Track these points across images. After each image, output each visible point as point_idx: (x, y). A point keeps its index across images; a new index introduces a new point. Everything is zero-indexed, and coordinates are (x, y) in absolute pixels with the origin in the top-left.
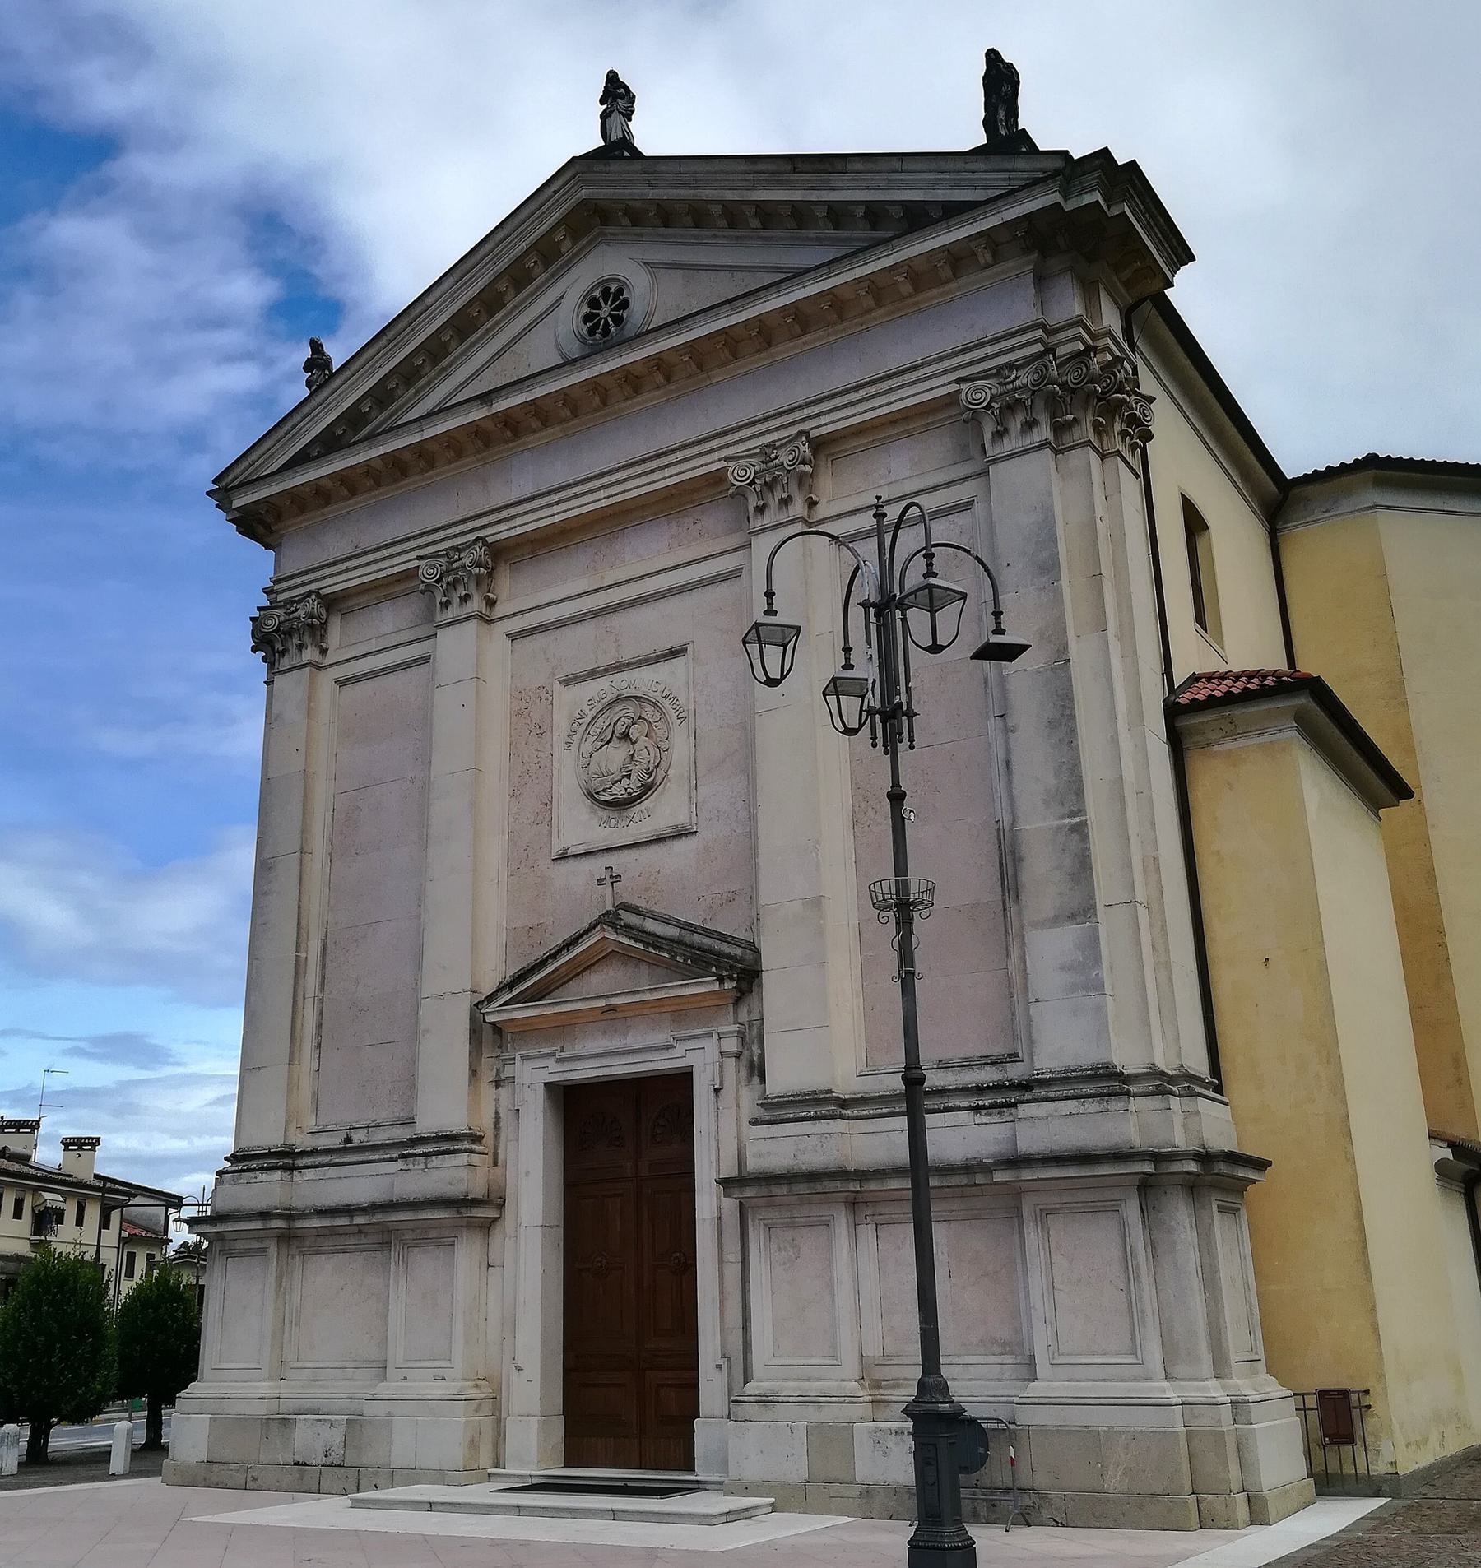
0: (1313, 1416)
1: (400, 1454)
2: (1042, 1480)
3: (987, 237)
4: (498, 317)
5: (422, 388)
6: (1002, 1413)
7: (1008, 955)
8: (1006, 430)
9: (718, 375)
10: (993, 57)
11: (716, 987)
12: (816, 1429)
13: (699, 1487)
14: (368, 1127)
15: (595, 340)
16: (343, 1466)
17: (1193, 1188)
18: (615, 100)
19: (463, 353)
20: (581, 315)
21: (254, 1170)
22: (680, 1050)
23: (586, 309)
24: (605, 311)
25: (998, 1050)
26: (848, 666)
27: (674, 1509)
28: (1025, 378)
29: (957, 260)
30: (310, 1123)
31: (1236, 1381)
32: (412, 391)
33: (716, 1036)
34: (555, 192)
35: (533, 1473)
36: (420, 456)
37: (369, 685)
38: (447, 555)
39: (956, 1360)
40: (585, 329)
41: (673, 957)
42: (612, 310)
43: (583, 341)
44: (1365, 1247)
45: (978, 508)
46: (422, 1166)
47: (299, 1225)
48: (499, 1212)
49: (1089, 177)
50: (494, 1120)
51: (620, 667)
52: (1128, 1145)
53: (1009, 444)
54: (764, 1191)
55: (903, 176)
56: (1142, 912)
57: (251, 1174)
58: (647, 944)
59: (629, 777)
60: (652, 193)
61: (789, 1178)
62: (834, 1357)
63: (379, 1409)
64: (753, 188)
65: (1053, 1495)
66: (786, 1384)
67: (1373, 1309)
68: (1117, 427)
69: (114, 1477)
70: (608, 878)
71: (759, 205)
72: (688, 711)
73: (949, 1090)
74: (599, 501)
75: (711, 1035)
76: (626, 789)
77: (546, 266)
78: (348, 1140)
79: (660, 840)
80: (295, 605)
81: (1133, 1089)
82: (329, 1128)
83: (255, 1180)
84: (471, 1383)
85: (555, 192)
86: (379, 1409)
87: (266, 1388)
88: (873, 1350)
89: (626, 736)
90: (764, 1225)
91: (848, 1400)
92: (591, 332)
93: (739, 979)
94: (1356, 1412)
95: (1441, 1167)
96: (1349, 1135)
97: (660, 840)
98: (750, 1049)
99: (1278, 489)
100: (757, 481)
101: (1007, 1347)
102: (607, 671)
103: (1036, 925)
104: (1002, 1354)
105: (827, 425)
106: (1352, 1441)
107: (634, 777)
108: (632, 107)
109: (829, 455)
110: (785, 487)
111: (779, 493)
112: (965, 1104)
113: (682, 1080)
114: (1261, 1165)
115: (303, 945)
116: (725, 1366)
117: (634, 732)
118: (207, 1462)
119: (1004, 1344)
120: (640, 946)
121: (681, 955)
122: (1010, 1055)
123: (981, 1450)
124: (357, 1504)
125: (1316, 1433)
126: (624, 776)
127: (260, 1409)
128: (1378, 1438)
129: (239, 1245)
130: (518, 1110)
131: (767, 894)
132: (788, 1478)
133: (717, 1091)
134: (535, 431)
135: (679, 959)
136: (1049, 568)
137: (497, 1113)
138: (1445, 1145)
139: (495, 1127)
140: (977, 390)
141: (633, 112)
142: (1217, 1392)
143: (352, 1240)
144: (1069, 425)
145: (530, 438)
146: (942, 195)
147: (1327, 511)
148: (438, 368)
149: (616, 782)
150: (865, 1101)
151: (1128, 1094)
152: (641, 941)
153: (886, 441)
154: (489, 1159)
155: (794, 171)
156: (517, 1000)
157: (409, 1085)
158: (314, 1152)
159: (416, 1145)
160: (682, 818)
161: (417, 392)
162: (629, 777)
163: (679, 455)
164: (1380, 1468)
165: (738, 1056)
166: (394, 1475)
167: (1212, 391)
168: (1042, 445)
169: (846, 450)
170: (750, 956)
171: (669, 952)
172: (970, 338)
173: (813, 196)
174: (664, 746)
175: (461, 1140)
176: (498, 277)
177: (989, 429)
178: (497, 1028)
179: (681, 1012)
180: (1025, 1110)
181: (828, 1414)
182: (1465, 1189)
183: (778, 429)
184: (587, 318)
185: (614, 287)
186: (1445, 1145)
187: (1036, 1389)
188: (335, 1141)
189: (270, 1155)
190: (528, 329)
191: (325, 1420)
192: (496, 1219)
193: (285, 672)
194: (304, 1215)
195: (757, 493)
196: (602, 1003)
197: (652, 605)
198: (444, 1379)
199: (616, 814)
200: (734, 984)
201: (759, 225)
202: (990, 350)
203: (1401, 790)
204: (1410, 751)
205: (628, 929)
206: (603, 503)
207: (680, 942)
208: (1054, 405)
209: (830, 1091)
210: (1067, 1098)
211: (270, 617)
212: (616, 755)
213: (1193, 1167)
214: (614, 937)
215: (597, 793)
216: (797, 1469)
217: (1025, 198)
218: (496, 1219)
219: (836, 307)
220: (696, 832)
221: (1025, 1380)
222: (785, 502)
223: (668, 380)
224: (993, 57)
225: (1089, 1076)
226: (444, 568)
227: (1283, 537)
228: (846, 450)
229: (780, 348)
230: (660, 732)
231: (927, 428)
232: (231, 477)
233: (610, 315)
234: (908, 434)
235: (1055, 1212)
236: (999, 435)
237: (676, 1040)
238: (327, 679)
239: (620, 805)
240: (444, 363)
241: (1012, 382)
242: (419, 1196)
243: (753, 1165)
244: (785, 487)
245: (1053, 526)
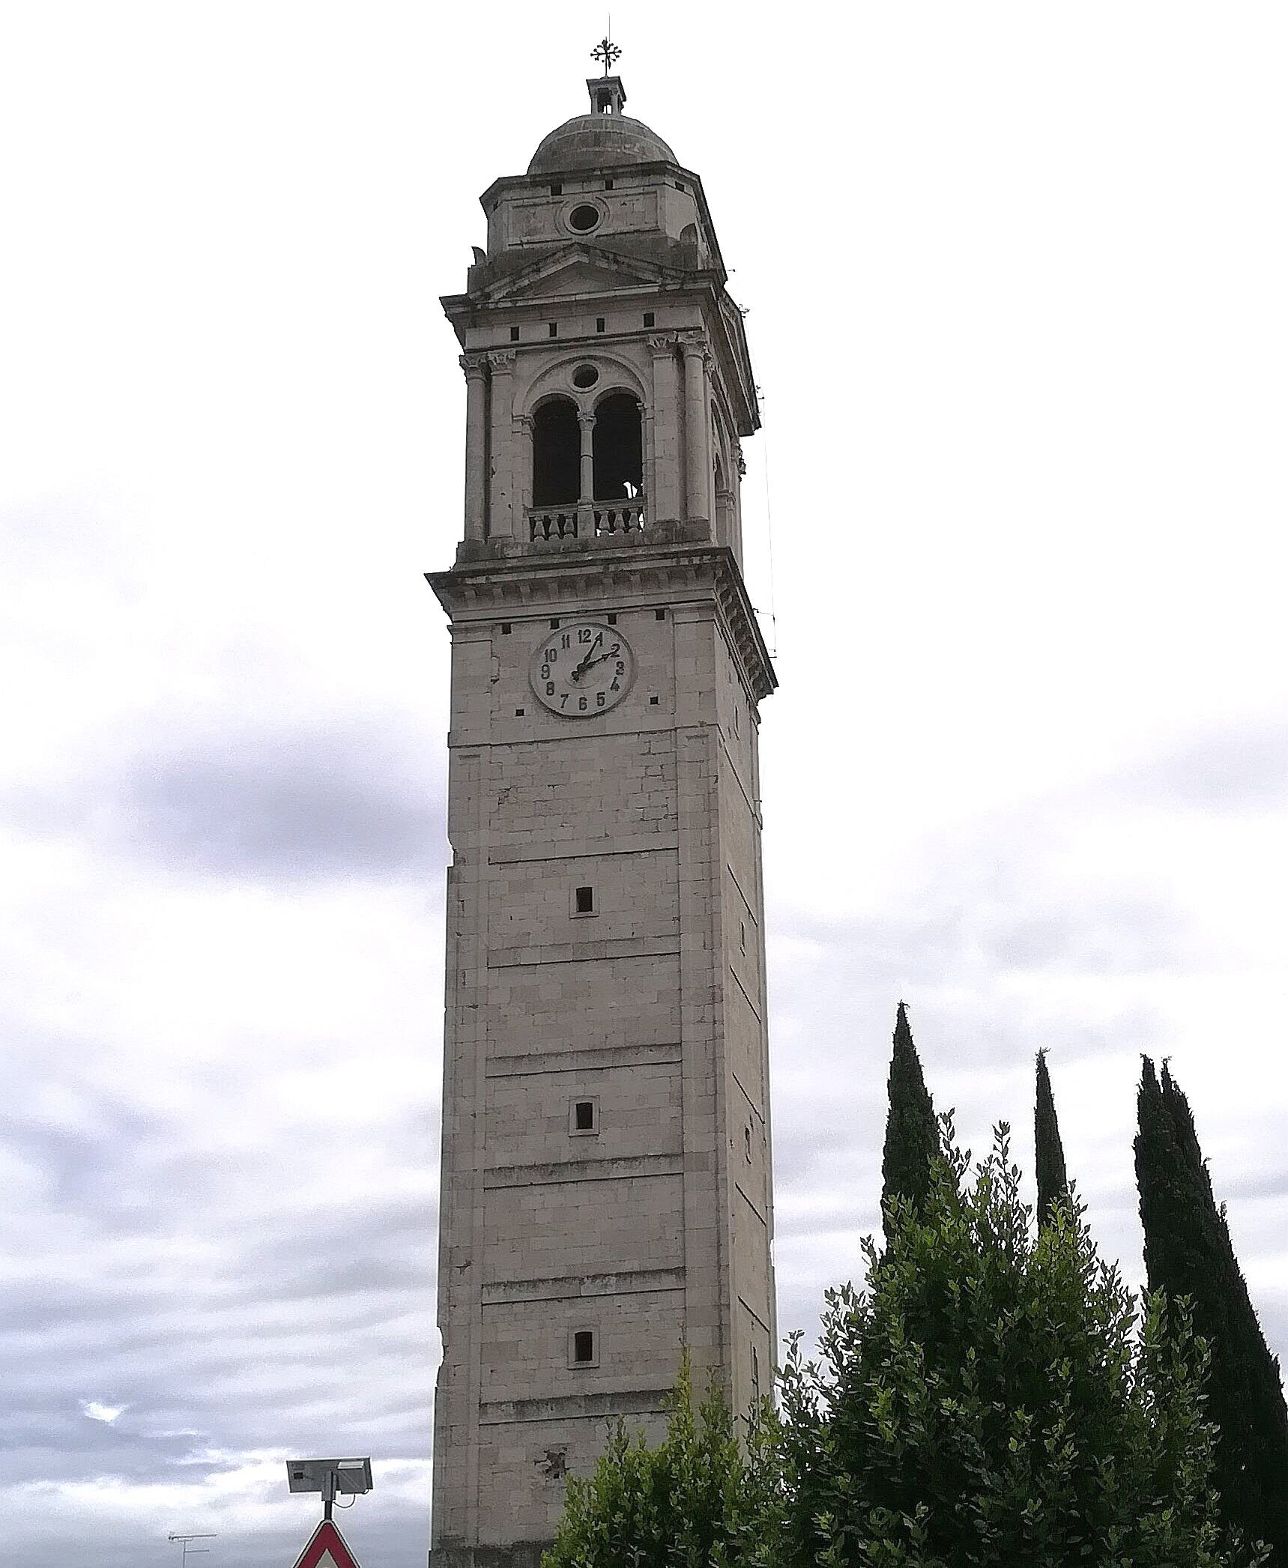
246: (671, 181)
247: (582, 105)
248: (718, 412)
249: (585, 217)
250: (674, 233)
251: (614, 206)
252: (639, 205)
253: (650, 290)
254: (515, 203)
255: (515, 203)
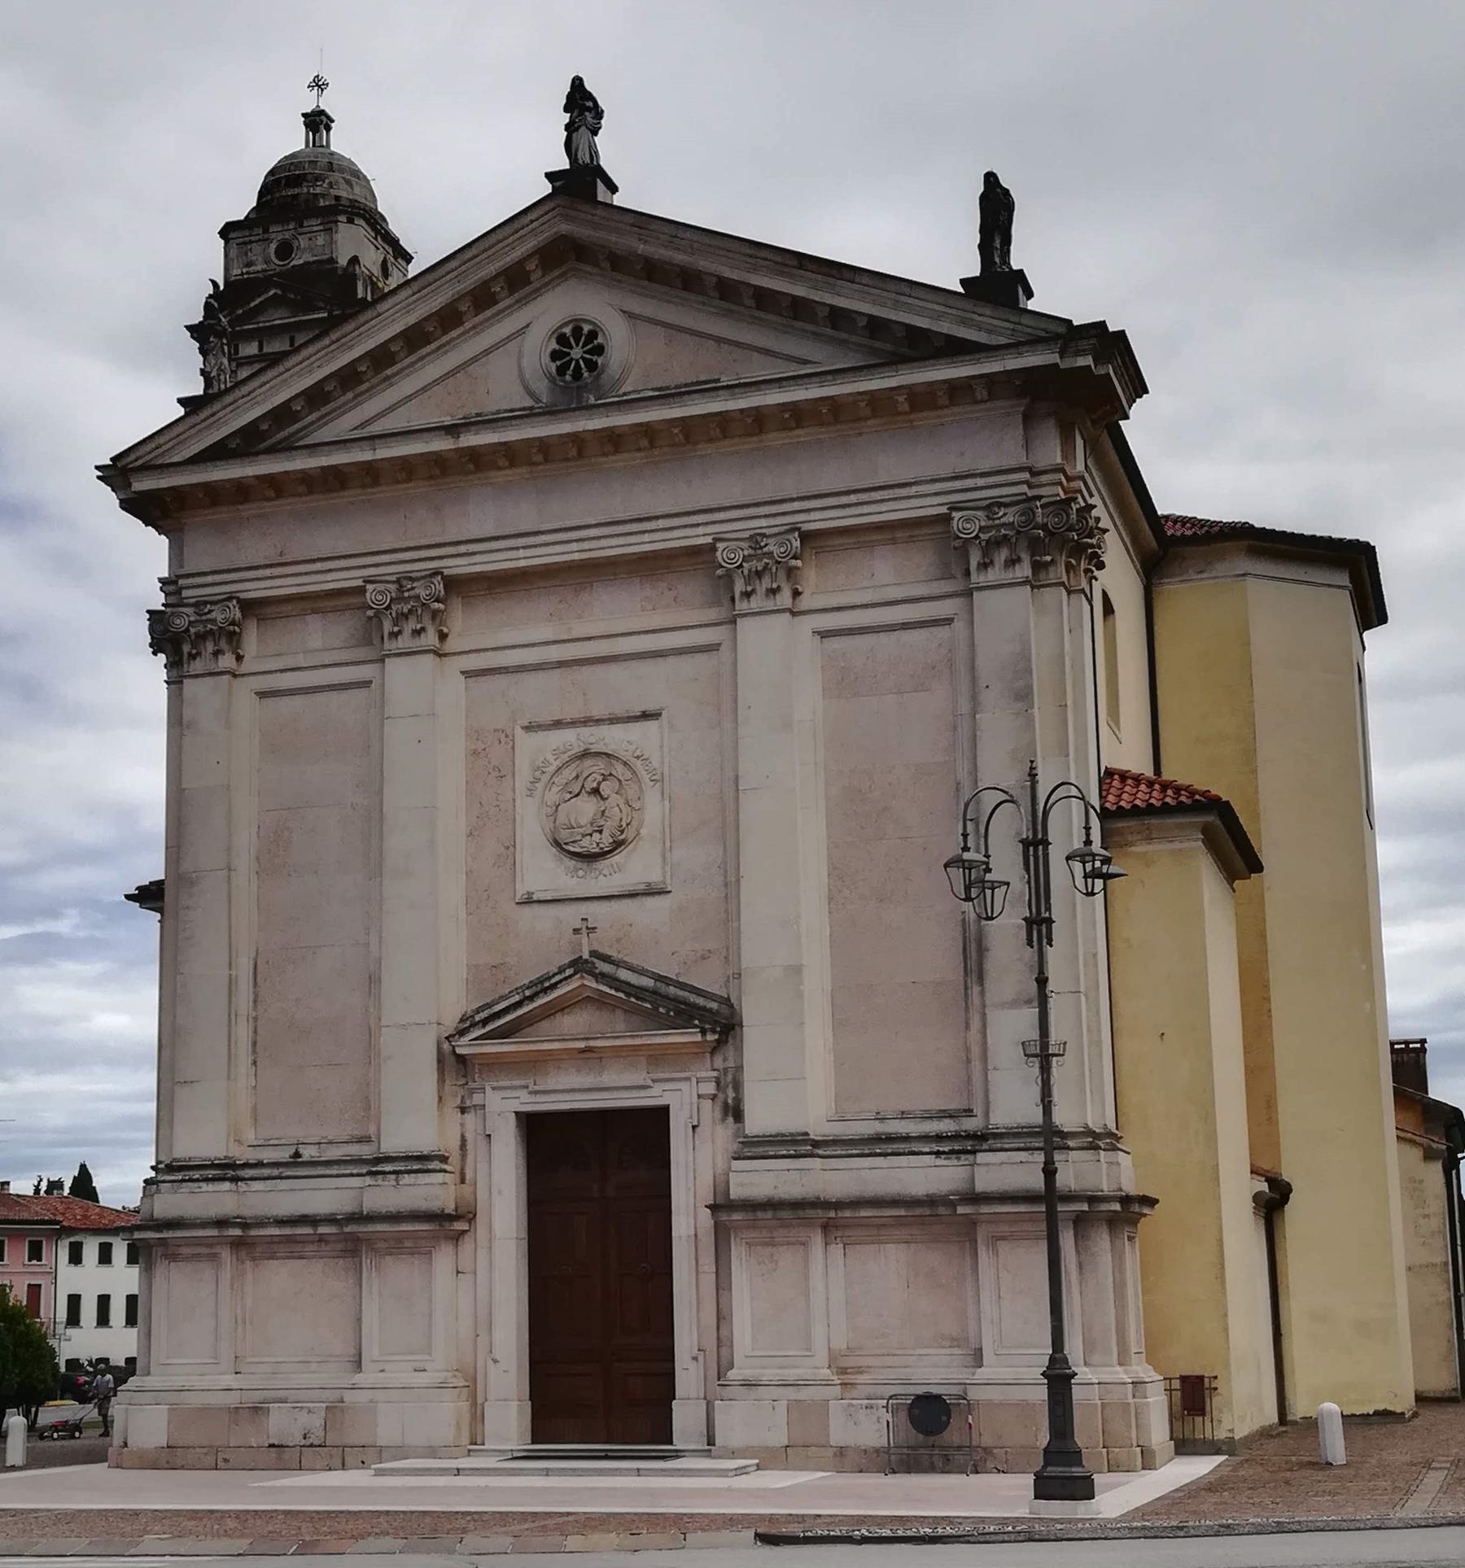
0: (1177, 1395)
1: (386, 1434)
2: (987, 1440)
3: (990, 381)
4: (454, 334)
5: (362, 393)
6: (955, 1390)
7: (967, 1026)
8: (992, 562)
9: (704, 449)
10: (991, 179)
11: (699, 1038)
12: (793, 1406)
13: (677, 1454)
14: (320, 1143)
15: (564, 381)
16: (325, 1446)
17: (1114, 1222)
18: (581, 114)
19: (412, 364)
20: (549, 350)
21: (197, 1180)
22: (657, 1089)
23: (554, 345)
24: (577, 353)
25: (952, 1106)
26: (966, 849)
27: (679, 1466)
28: (1010, 516)
29: (957, 391)
30: (250, 1136)
31: (1135, 1367)
32: (350, 395)
33: (694, 1080)
34: (532, 221)
35: (514, 1448)
36: (368, 473)
37: (297, 701)
38: (398, 581)
39: (911, 1352)
40: (553, 367)
41: (656, 1009)
42: (584, 352)
43: (552, 380)
44: (1223, 1267)
45: (959, 625)
46: (394, 1183)
47: (253, 1232)
48: (467, 1224)
49: (1085, 342)
50: (459, 1143)
51: (587, 721)
52: (1067, 1189)
53: (993, 575)
54: (750, 1216)
55: (910, 300)
56: (1083, 998)
57: (196, 1185)
58: (628, 994)
59: (601, 832)
60: (641, 248)
61: (772, 1205)
62: (809, 1349)
63: (362, 1397)
64: (754, 269)
65: (995, 1451)
66: (764, 1371)
67: (1226, 1315)
68: (1083, 566)
69: (13, 1468)
70: (584, 929)
71: (758, 289)
72: (662, 774)
73: (912, 1137)
74: (573, 553)
75: (688, 1079)
76: (598, 844)
77: (511, 293)
78: (297, 1155)
79: (632, 895)
80: (209, 606)
81: (1071, 1143)
82: (271, 1142)
83: (199, 1190)
84: (451, 1374)
85: (532, 221)
86: (362, 1397)
87: (229, 1380)
88: (840, 1344)
89: (596, 791)
90: (747, 1243)
91: (824, 1383)
92: (561, 371)
93: (720, 1033)
94: (1207, 1392)
95: (1257, 1197)
96: (1217, 1179)
97: (632, 895)
98: (725, 1092)
99: (1159, 545)
100: (744, 564)
101: (956, 1342)
102: (573, 723)
103: (1003, 1005)
104: (951, 1347)
105: (817, 521)
106: (1203, 1414)
107: (606, 833)
108: (599, 123)
109: (814, 548)
110: (774, 578)
111: (766, 582)
112: (927, 1150)
113: (661, 1115)
114: (1151, 1202)
115: (233, 964)
116: (701, 1358)
117: (605, 789)
118: (168, 1447)
119: (953, 1339)
120: (621, 995)
121: (664, 1007)
122: (965, 1111)
123: (944, 1418)
124: (380, 1473)
125: (1177, 1408)
126: (596, 831)
127: (232, 1399)
128: (1221, 1412)
129: (185, 1251)
130: (489, 1136)
131: (750, 957)
132: (770, 1444)
133: (694, 1127)
134: (499, 468)
135: (661, 1010)
136: (1024, 695)
137: (463, 1136)
138: (1263, 1179)
139: (461, 1149)
140: (968, 520)
141: (600, 128)
142: (1121, 1374)
143: (310, 1247)
144: (1047, 565)
145: (493, 473)
146: (945, 327)
147: (1201, 572)
148: (383, 375)
149: (587, 835)
150: (835, 1142)
151: (1069, 1148)
152: (622, 992)
153: (871, 545)
154: (457, 1177)
155: (800, 268)
156: (485, 1036)
157: (368, 1104)
158: (259, 1164)
159: (382, 1163)
160: (655, 877)
161: (355, 397)
162: (601, 832)
163: (661, 523)
164: (1221, 1434)
165: (714, 1098)
166: (381, 1452)
167: (1127, 474)
168: (1023, 582)
169: (832, 546)
170: (725, 1010)
171: (650, 1003)
172: (962, 467)
173: (816, 296)
174: (636, 805)
175: (432, 1161)
176: (461, 297)
177: (975, 558)
178: (462, 1060)
179: (658, 1057)
180: (981, 1157)
181: (805, 1394)
182: (1266, 1214)
183: (766, 516)
184: (555, 356)
185: (586, 328)
186: (1263, 1179)
187: (982, 1374)
188: (284, 1155)
189: (213, 1166)
190: (487, 352)
191: (302, 1407)
192: (464, 1232)
193: (197, 676)
194: (261, 1223)
195: (744, 577)
196: (582, 1045)
197: (624, 664)
198: (425, 1370)
199: (584, 866)
200: (716, 1037)
201: (754, 305)
202: (980, 482)
203: (1255, 866)
204: (1256, 817)
205: (601, 977)
206: (576, 556)
207: (655, 992)
208: (1035, 546)
209: (807, 1134)
210: (1019, 1149)
211: (179, 615)
212: (586, 808)
213: (1117, 1207)
214: (594, 985)
215: (565, 844)
216: (778, 1437)
217: (1028, 352)
218: (464, 1232)
219: (834, 412)
220: (670, 892)
221: (973, 1367)
222: (773, 592)
223: (652, 445)
224: (991, 179)
225: (1036, 1132)
226: (394, 595)
227: (1156, 590)
228: (832, 546)
229: (771, 436)
230: (631, 791)
231: (911, 539)
232: (129, 459)
233: (582, 358)
234: (894, 541)
235: (1003, 1238)
236: (984, 566)
237: (653, 1081)
238: (244, 690)
239: (590, 858)
240: (389, 372)
241: (999, 518)
242: (392, 1209)
243: (735, 1193)
244: (774, 578)
245: (1029, 660)
246: (342, 218)
247: (295, 140)
248: (972, 320)
249: (285, 250)
250: (343, 261)
251: (303, 242)
252: (321, 240)
253: (321, 315)
254: (238, 241)
255: (238, 241)
